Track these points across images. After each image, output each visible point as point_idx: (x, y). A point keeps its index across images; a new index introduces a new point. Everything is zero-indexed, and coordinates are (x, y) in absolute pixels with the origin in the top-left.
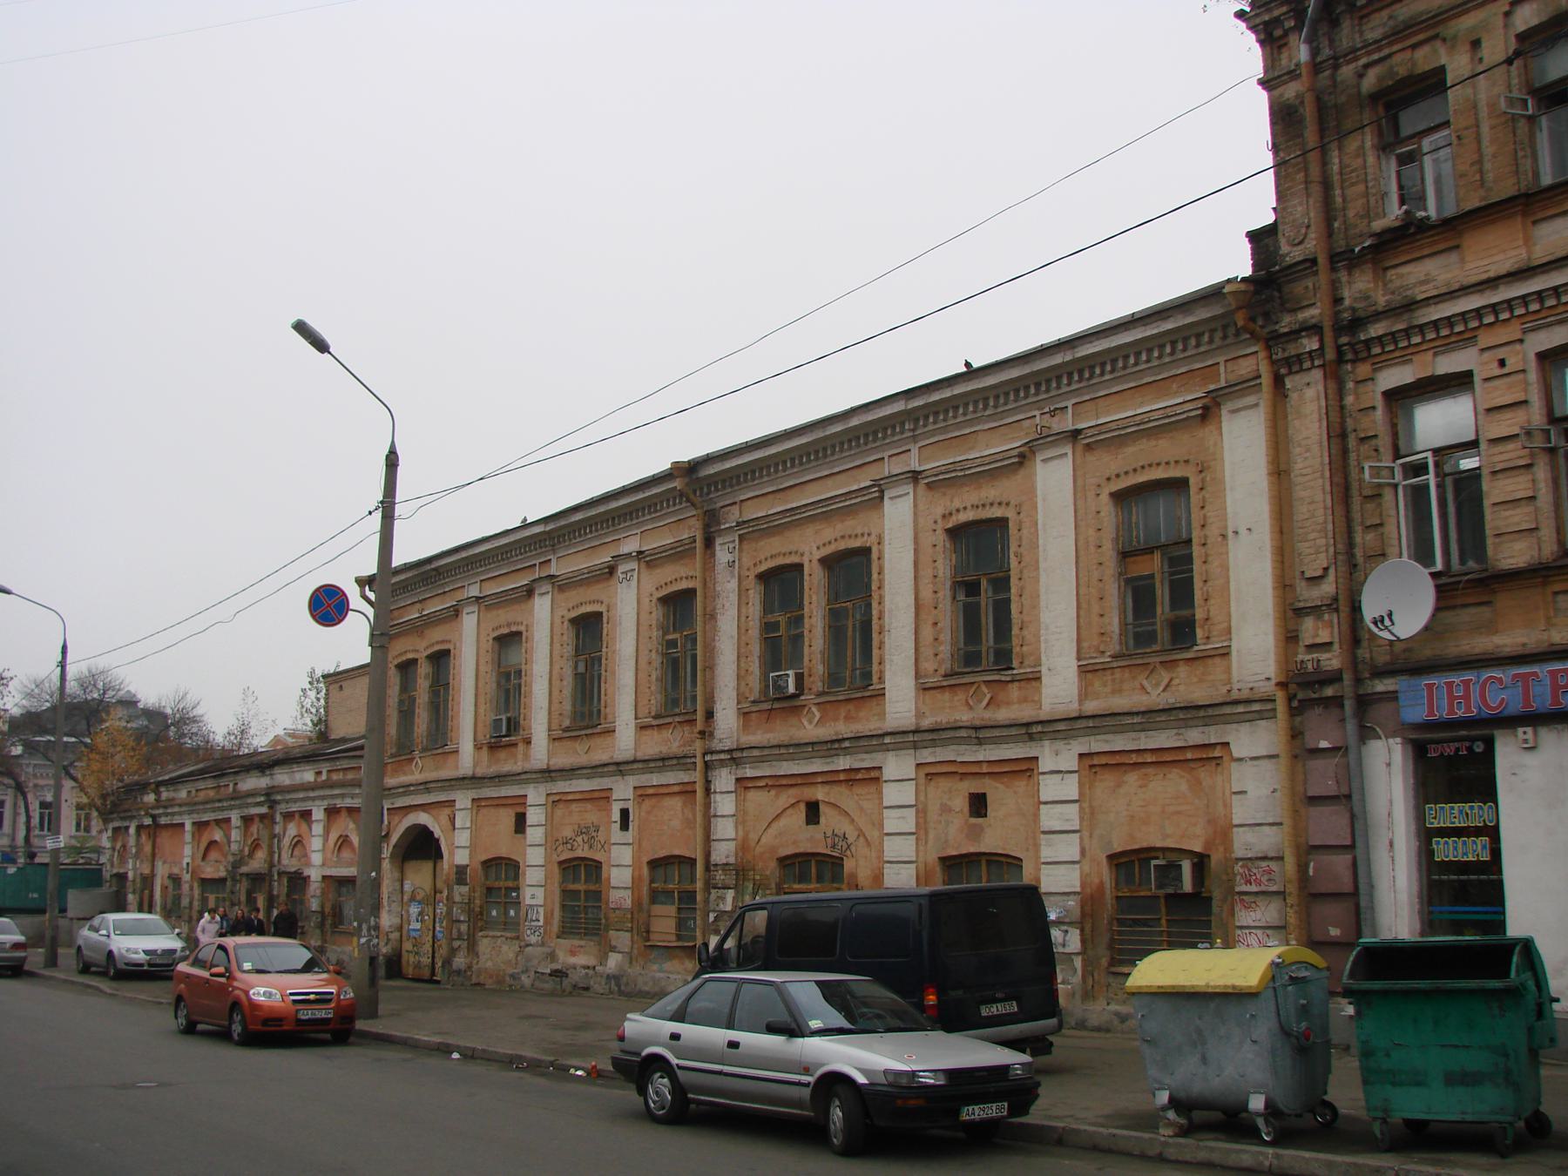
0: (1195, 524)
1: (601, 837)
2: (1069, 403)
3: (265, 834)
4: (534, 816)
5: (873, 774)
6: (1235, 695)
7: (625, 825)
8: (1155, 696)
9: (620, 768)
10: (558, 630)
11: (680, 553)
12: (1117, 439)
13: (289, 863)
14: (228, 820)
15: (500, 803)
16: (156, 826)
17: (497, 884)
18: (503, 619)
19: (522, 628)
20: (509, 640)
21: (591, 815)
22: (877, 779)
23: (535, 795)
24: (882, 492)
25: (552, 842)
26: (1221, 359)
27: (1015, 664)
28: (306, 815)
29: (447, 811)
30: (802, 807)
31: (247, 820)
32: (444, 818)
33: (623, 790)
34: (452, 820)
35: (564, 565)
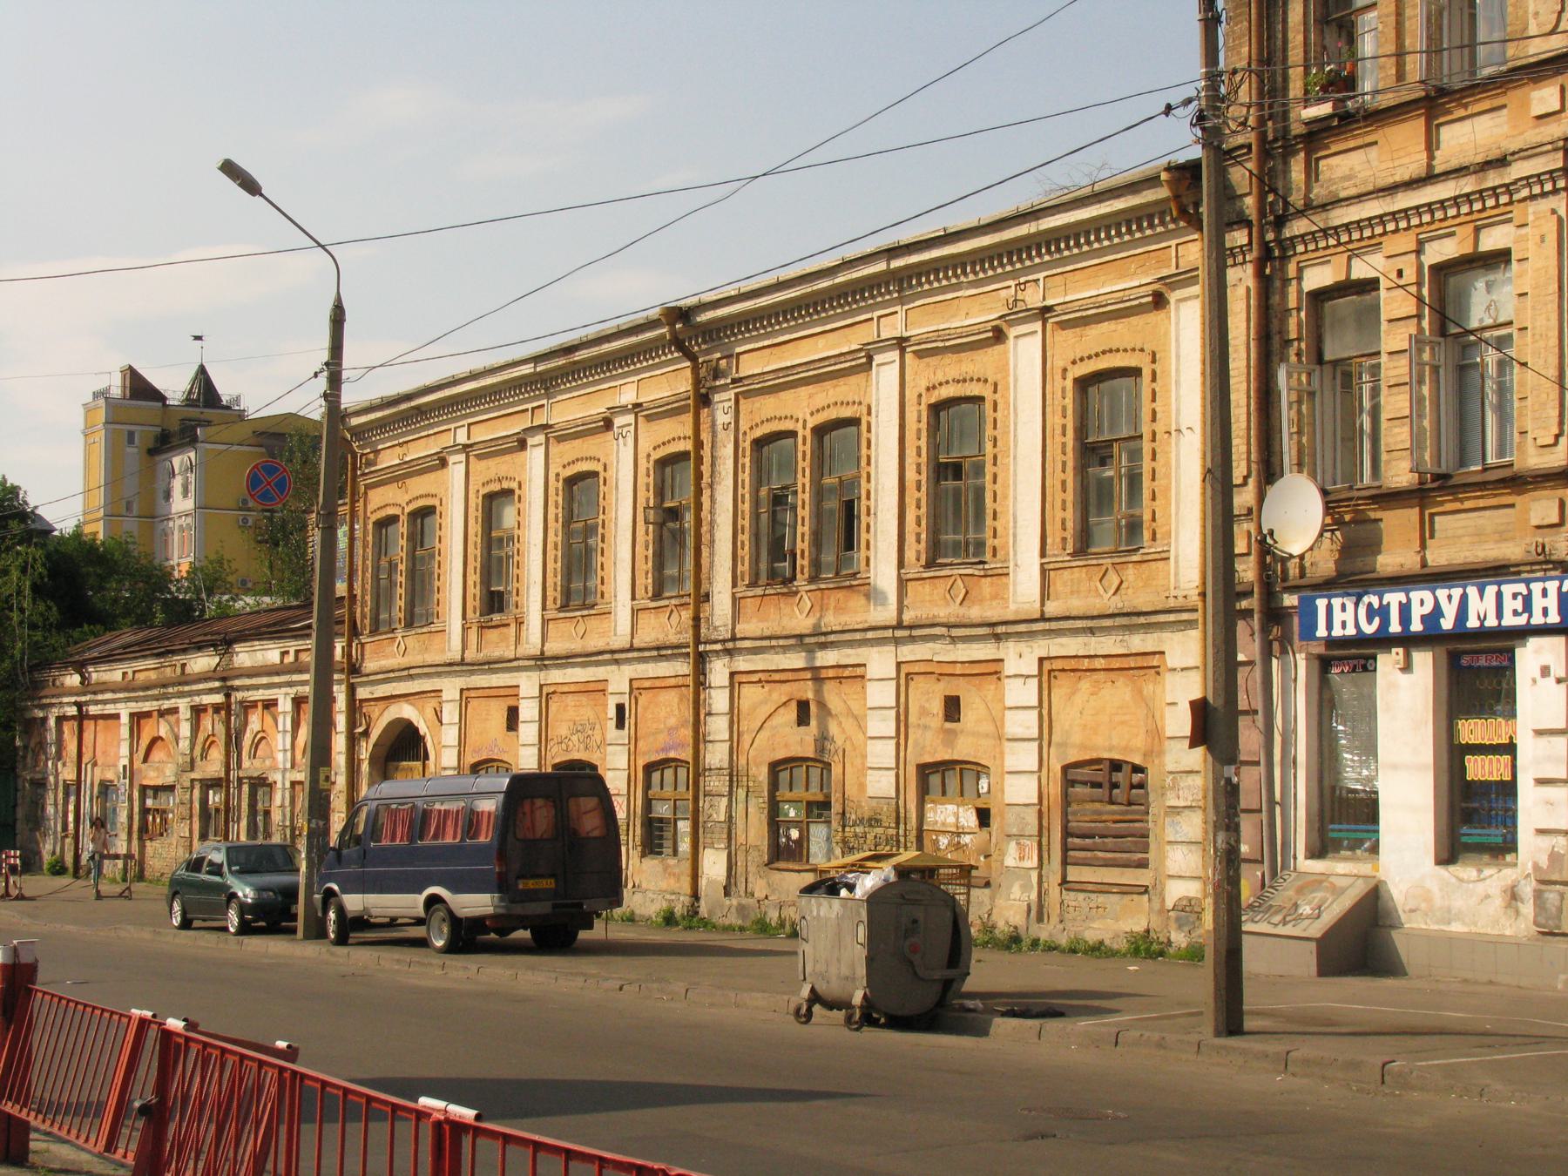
0: (1145, 415)
2: (1041, 276)
3: (220, 729)
4: (528, 711)
5: (859, 671)
6: (1172, 603)
7: (620, 724)
9: (614, 656)
10: (641, 503)
11: (670, 411)
13: (250, 766)
14: (175, 711)
15: (491, 694)
16: (82, 717)
18: (489, 472)
19: (514, 485)
20: (495, 500)
21: (587, 713)
22: (863, 677)
23: (528, 684)
24: (870, 358)
26: (1173, 243)
27: (988, 556)
28: (270, 705)
29: (433, 703)
30: (794, 705)
31: (198, 711)
32: (430, 712)
33: (618, 679)
34: (438, 715)
35: (568, 409)
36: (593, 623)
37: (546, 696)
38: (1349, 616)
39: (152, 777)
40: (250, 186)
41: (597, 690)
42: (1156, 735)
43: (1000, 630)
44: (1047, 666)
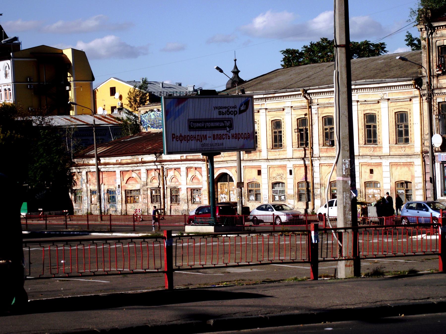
1: (284, 176)
6: (415, 154)
8: (402, 152)
12: (397, 100)
17: (252, 189)
21: (281, 171)
25: (269, 177)
36: (281, 152)
37: (269, 168)
38: (255, 256)
39: (129, 187)
40: (221, 71)
41: (284, 167)
42: (413, 177)
43: (381, 157)
44: (391, 164)
